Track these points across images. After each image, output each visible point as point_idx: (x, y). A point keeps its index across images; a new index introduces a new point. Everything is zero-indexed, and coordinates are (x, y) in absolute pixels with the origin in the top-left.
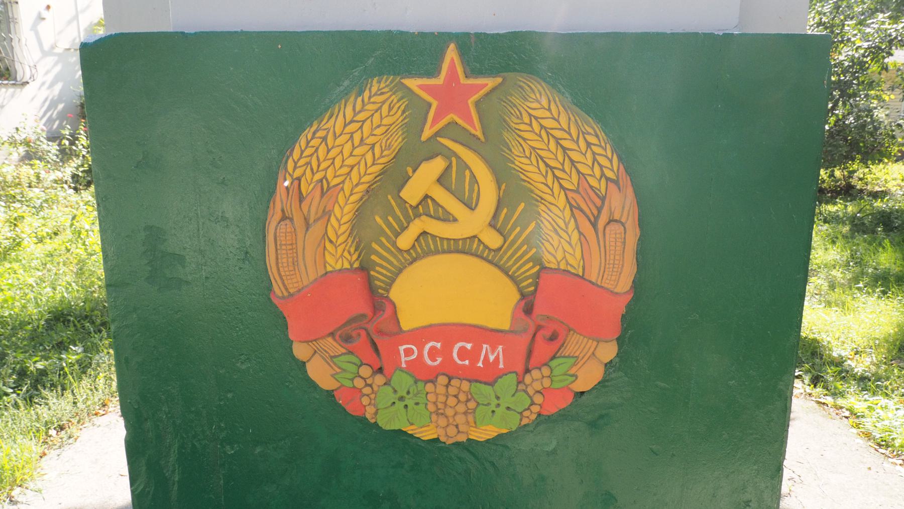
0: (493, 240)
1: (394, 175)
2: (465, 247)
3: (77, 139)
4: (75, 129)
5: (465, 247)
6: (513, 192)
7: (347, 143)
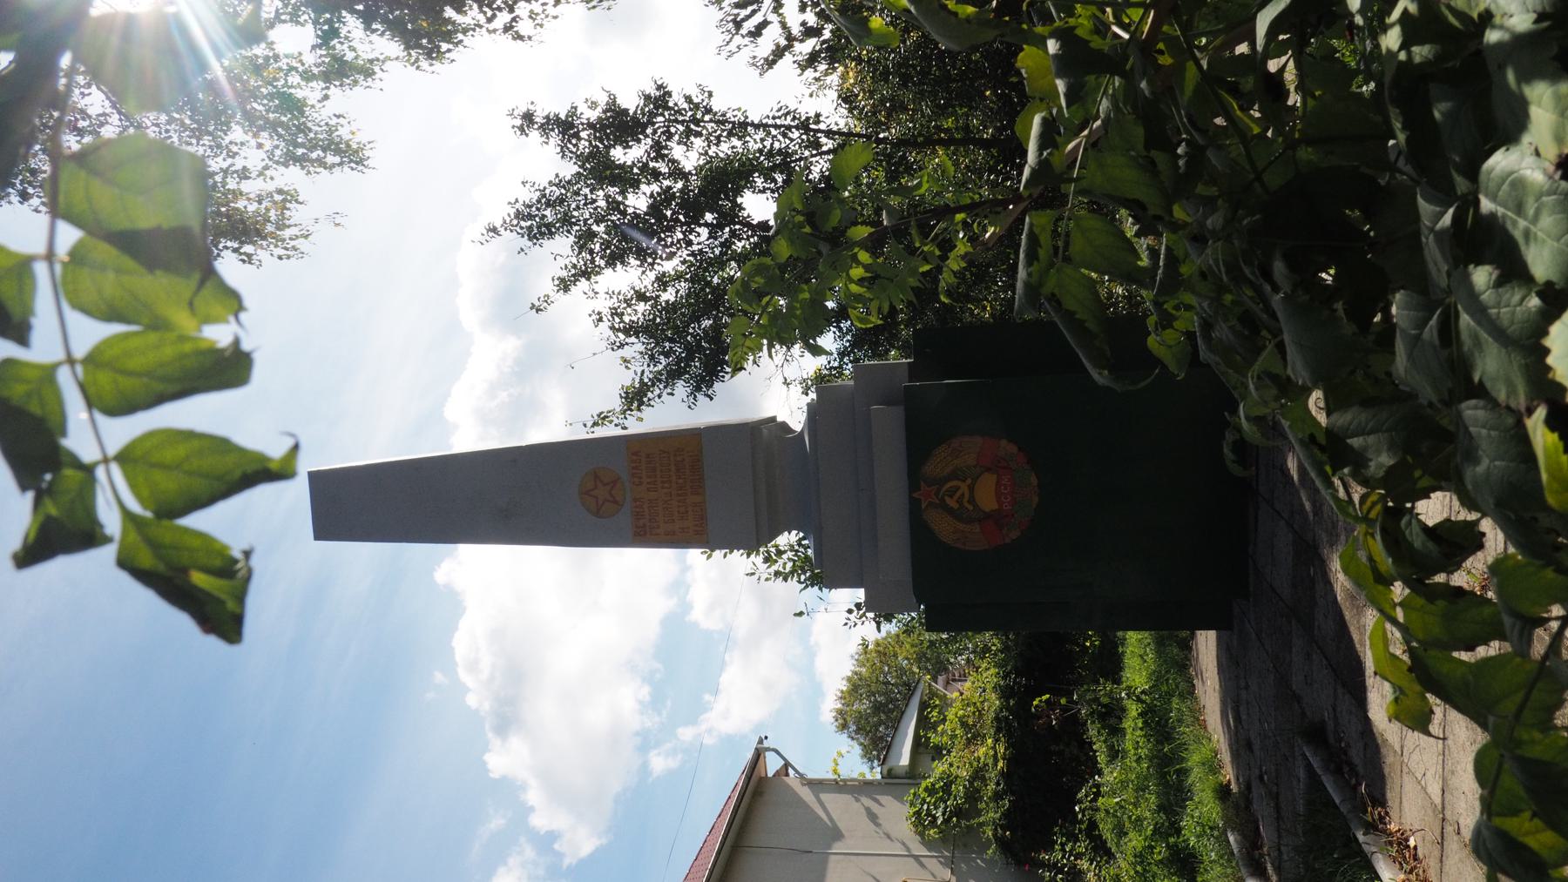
0: (969, 481)
1: (950, 511)
2: (971, 488)
3: (1055, 864)
4: (1043, 865)
5: (971, 488)
6: (954, 475)
7: (944, 527)
